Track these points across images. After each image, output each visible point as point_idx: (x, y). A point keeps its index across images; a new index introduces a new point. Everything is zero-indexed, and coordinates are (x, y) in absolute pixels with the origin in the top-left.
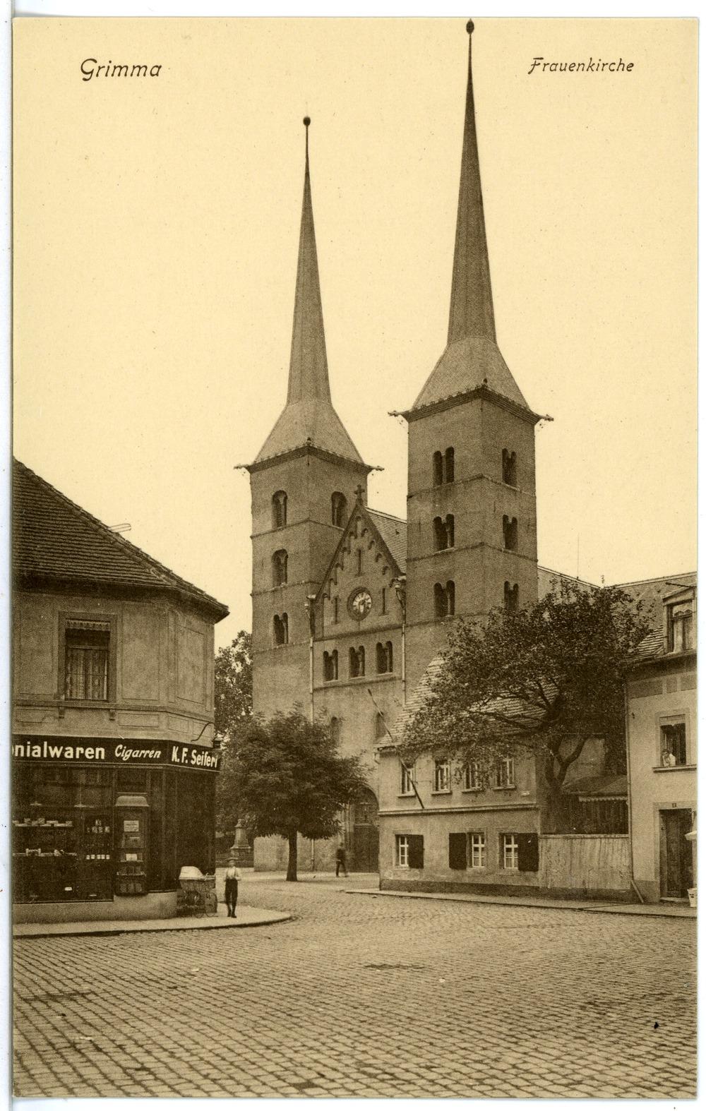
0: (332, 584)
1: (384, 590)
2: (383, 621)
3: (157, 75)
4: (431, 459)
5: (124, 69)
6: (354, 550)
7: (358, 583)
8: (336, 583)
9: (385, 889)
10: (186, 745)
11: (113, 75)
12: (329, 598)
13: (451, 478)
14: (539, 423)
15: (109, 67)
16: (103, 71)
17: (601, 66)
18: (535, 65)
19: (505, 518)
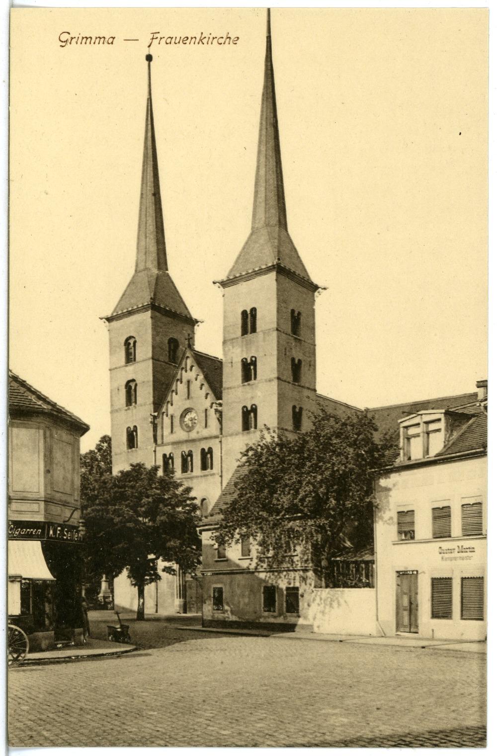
0: (169, 405)
1: (206, 410)
2: (205, 433)
3: (112, 43)
4: (240, 316)
5: (89, 39)
6: (184, 380)
7: (188, 404)
8: (172, 405)
9: (206, 627)
10: (60, 525)
11: (94, 43)
12: (167, 416)
13: (254, 330)
14: (318, 291)
15: (209, 38)
16: (74, 41)
17: (211, 38)
18: (153, 38)
19: (293, 360)
